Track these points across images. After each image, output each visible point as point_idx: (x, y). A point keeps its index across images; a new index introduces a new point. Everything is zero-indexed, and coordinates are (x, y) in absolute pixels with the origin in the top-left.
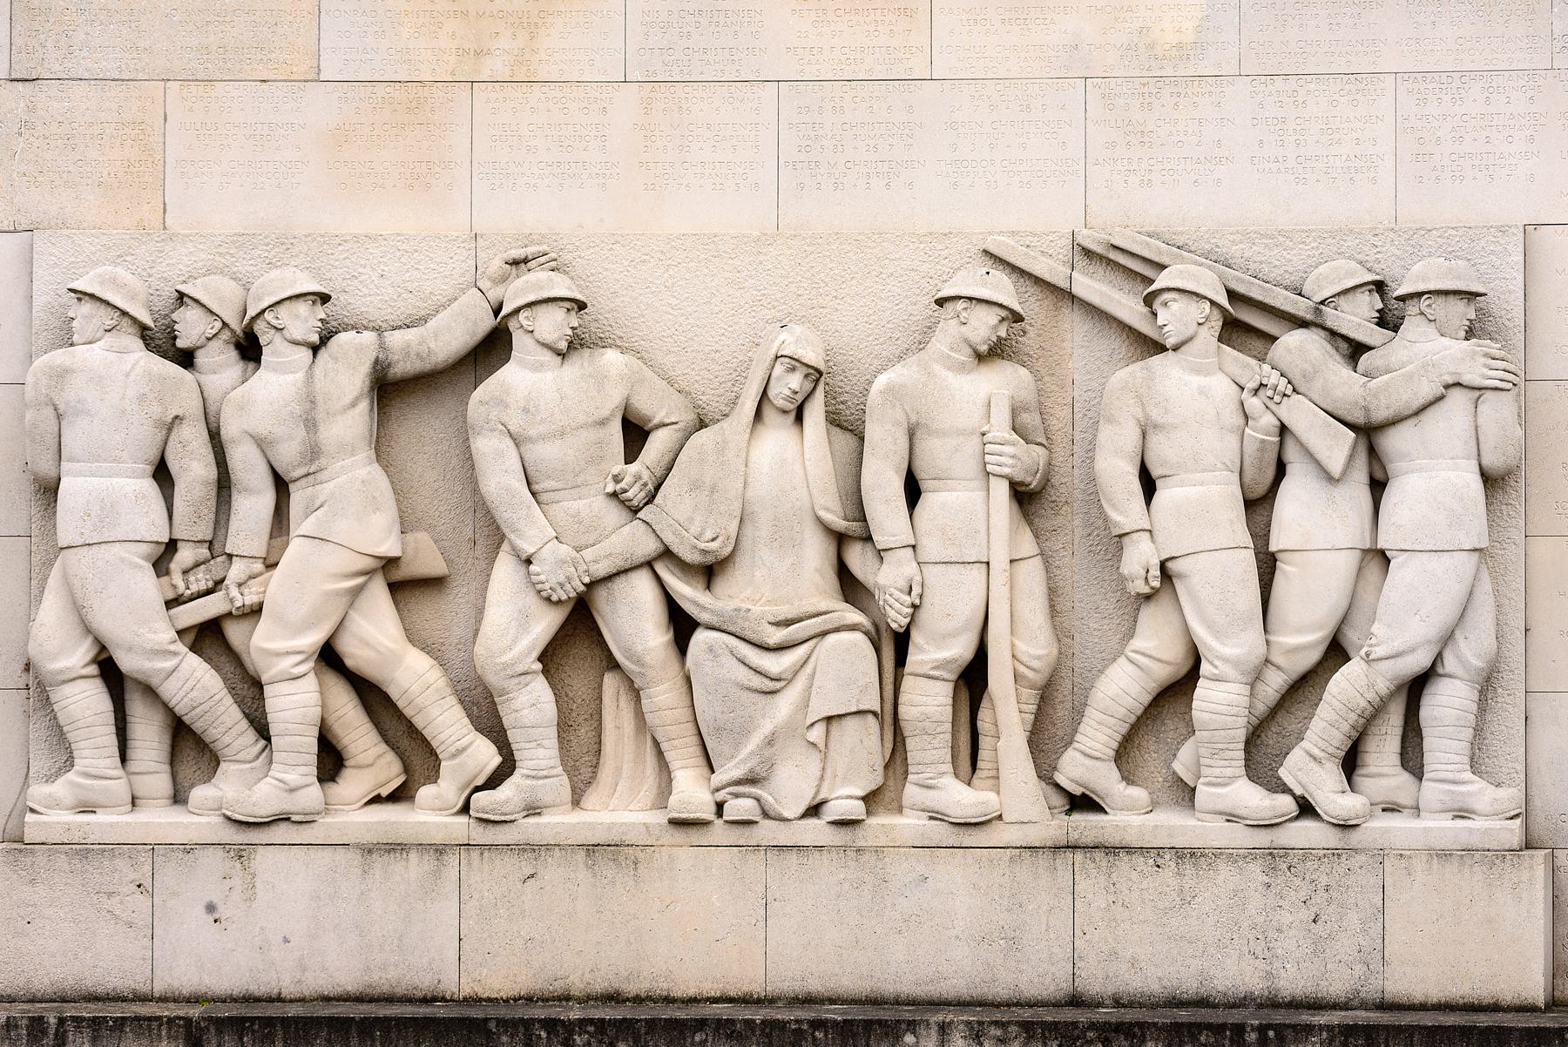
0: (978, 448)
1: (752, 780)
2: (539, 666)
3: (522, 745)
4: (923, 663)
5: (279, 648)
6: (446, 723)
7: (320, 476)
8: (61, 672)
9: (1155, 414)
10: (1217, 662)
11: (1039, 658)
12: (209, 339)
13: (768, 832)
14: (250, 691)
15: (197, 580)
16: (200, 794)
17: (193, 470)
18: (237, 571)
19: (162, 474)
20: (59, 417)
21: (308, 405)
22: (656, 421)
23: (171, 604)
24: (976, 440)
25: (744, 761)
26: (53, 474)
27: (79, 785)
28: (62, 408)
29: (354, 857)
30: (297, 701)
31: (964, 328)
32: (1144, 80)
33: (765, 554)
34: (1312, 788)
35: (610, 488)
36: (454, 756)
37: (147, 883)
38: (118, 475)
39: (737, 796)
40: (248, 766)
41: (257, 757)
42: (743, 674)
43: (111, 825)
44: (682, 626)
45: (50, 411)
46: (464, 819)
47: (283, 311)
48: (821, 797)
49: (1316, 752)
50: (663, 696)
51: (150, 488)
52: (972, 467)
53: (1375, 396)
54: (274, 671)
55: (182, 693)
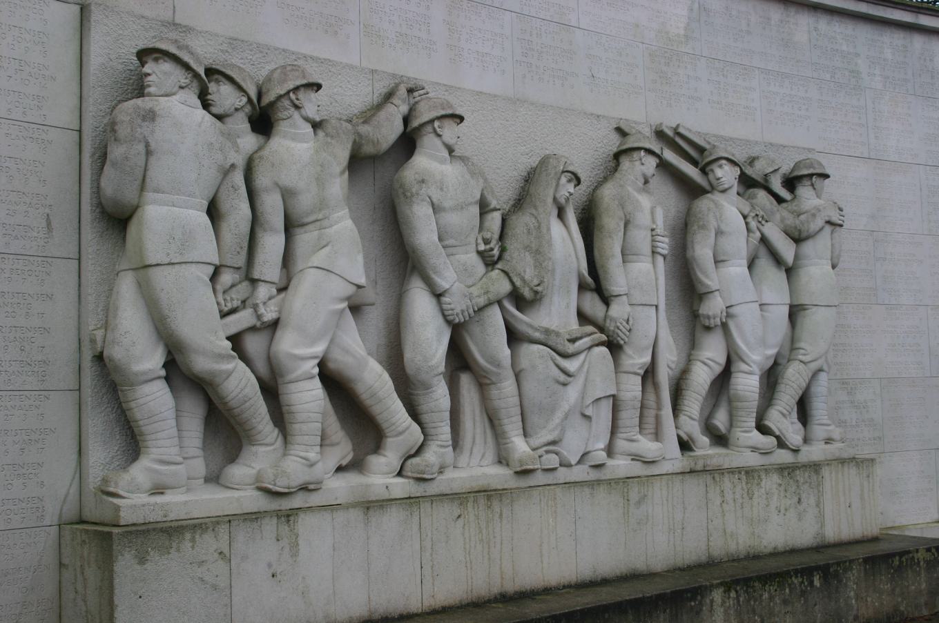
0: (649, 238)
1: (554, 443)
2: (163, 373)
3: (146, 421)
4: (633, 365)
5: (299, 350)
6: (393, 410)
7: (325, 223)
8: (144, 373)
9: (723, 227)
10: (752, 364)
11: (673, 362)
12: (237, 110)
13: (563, 475)
14: (271, 390)
15: (232, 299)
16: (239, 472)
17: (238, 212)
18: (263, 291)
19: (213, 212)
20: (149, 153)
21: (319, 168)
22: (492, 207)
23: (224, 315)
24: (649, 233)
25: (553, 430)
26: (135, 202)
27: (156, 471)
28: (153, 145)
29: (355, 515)
30: (308, 397)
31: (642, 167)
32: (666, 50)
33: (556, 299)
34: (784, 431)
35: (482, 247)
36: (397, 436)
37: (226, 551)
38: (191, 208)
39: (547, 452)
40: (272, 448)
41: (276, 440)
42: (556, 372)
43: (186, 503)
44: (514, 337)
45: (141, 148)
46: (400, 480)
47: (301, 94)
48: (588, 450)
49: (785, 412)
50: (506, 390)
51: (206, 219)
52: (648, 250)
53: (803, 224)
54: (299, 372)
55: (239, 390)
